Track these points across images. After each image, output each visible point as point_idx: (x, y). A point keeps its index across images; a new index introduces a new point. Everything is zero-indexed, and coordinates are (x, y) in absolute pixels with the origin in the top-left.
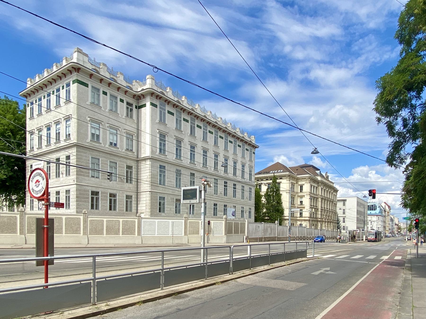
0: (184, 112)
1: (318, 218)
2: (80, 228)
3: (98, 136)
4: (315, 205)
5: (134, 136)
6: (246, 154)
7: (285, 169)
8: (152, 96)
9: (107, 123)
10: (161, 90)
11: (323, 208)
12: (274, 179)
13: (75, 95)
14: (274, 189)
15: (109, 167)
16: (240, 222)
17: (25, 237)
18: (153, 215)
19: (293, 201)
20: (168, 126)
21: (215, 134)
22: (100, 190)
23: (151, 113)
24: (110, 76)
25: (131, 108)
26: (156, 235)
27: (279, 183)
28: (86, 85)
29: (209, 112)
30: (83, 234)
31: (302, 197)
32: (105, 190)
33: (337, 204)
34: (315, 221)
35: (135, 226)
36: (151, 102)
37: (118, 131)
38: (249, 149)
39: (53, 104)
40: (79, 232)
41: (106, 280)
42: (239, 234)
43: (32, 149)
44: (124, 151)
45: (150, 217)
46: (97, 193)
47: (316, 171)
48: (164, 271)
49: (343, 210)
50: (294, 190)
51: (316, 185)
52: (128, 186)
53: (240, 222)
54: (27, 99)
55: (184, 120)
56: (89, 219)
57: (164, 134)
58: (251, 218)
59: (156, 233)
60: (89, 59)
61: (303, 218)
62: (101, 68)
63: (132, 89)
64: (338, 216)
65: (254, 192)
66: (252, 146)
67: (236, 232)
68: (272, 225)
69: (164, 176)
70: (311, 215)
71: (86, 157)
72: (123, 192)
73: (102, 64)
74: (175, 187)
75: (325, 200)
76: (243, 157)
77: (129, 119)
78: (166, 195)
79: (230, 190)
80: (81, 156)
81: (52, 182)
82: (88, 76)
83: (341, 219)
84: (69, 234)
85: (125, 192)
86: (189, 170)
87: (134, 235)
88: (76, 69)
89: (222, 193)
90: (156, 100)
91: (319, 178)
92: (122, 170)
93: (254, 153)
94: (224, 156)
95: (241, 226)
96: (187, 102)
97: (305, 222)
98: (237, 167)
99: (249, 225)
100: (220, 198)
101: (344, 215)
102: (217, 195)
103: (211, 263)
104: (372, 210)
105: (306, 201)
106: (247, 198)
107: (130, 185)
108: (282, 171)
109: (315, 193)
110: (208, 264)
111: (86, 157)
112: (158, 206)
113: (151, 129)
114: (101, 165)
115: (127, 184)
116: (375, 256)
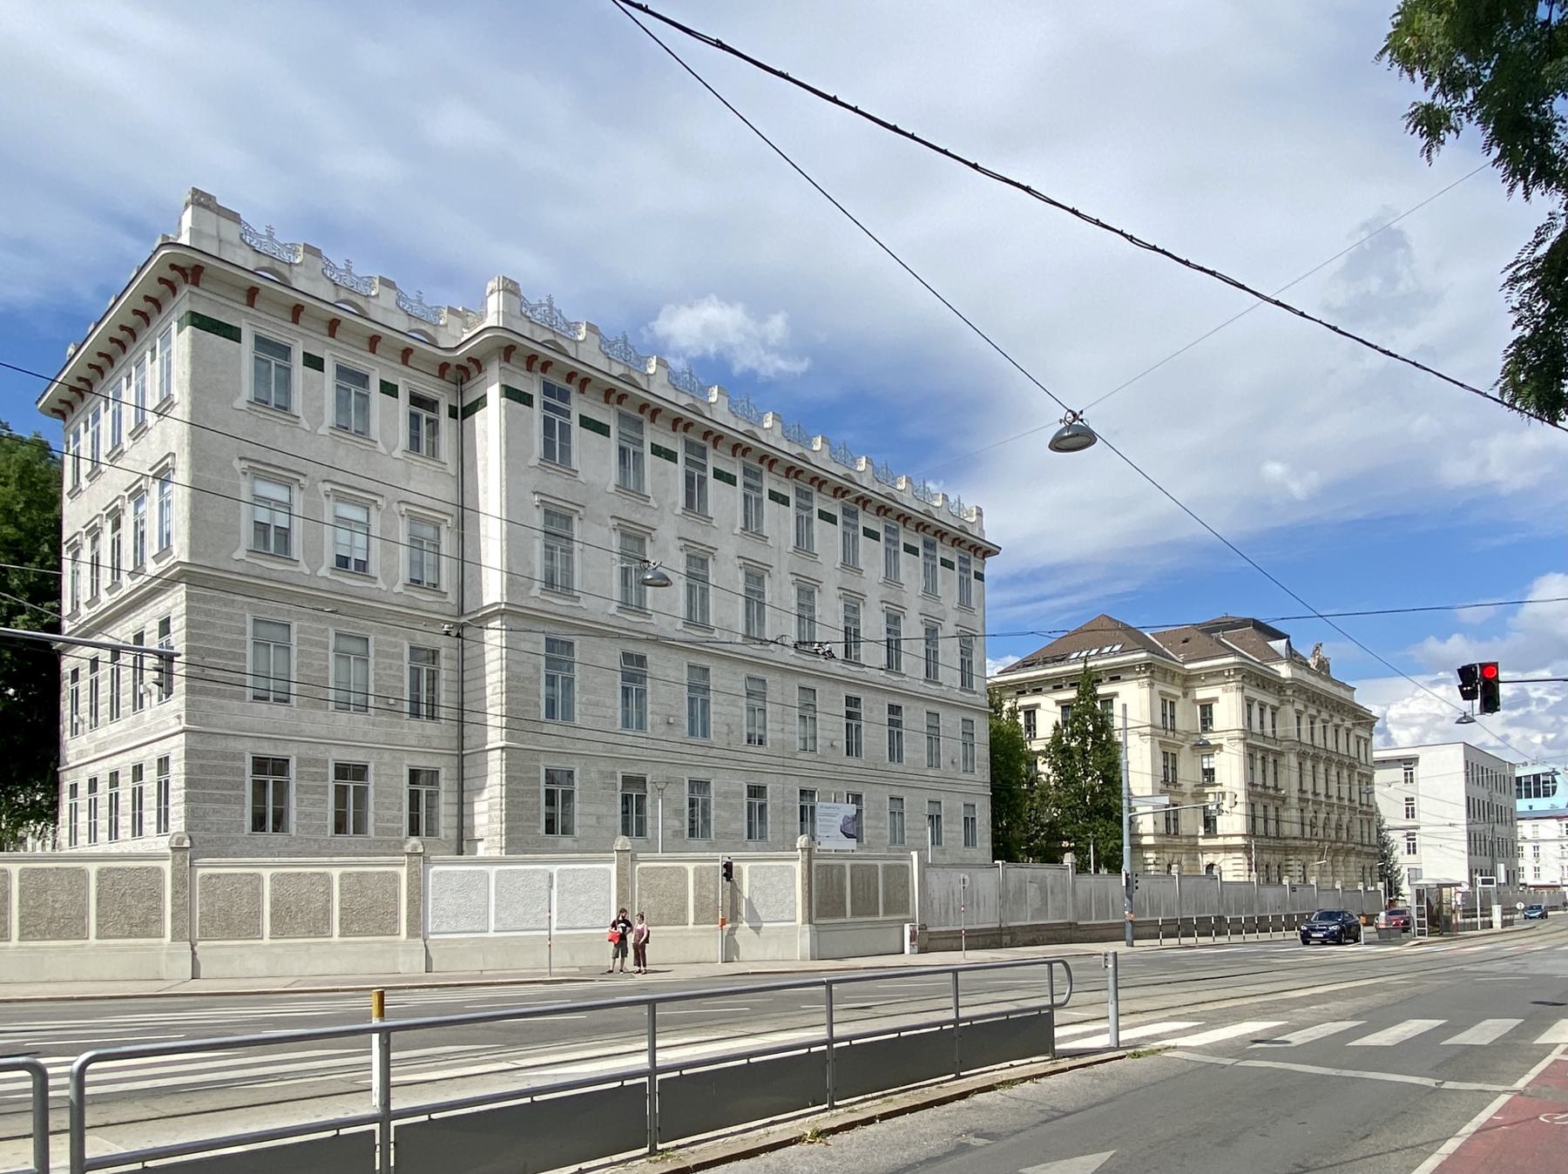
0: (715, 447)
1: (1285, 838)
2: (159, 911)
3: (284, 534)
4: (1271, 782)
5: (443, 528)
6: (944, 583)
7: (1135, 638)
8: (507, 359)
9: (324, 481)
10: (749, 427)
11: (1310, 796)
12: (1087, 681)
13: (184, 373)
14: (1084, 724)
15: (331, 655)
16: (880, 863)
17: (425, 946)
18: (516, 842)
19: (1174, 769)
20: (581, 477)
21: (798, 506)
22: (292, 753)
23: (503, 427)
24: (337, 295)
25: (432, 416)
26: (491, 934)
27: (1108, 700)
28: (233, 334)
29: (583, 329)
30: (173, 936)
31: (1207, 749)
32: (319, 753)
33: (1375, 775)
34: (1274, 850)
35: (396, 896)
36: (502, 386)
37: (373, 509)
38: (955, 560)
39: (129, 426)
40: (154, 929)
41: (681, 1074)
42: (880, 918)
43: (76, 604)
44: (398, 588)
45: (504, 855)
46: (280, 766)
47: (1270, 643)
48: (659, 1077)
49: (1407, 799)
50: (1173, 723)
51: (1271, 700)
52: (419, 731)
53: (880, 863)
54: (65, 420)
55: (586, 422)
56: (200, 872)
57: (568, 513)
58: (974, 845)
59: (492, 926)
60: (246, 231)
61: (1220, 842)
62: (297, 265)
63: (436, 342)
64: (1384, 827)
65: (986, 739)
66: (971, 547)
67: (865, 906)
68: (1047, 872)
69: (569, 683)
70: (1254, 826)
71: (230, 617)
72: (398, 755)
73: (377, 282)
74: (543, 717)
75: (1316, 758)
76: (930, 590)
77: (419, 462)
78: (576, 761)
79: (874, 736)
80: (206, 615)
81: (124, 730)
82: (238, 299)
83: (1398, 839)
84: (116, 937)
85: (405, 755)
86: (920, 704)
87: (392, 938)
88: (189, 272)
89: (835, 744)
90: (528, 374)
91: (1284, 671)
92: (391, 668)
93: (979, 576)
94: (841, 592)
95: (886, 884)
96: (729, 409)
97: (1230, 856)
98: (768, 598)
99: (928, 874)
100: (827, 767)
101: (1411, 822)
102: (761, 750)
103: (850, 1038)
104: (1537, 795)
105: (1230, 768)
106: (953, 762)
107: (429, 727)
108: (1117, 648)
109: (1268, 730)
110: (835, 1046)
111: (230, 617)
112: (539, 809)
113: (504, 494)
114: (299, 651)
115: (415, 723)
116: (1507, 1024)
